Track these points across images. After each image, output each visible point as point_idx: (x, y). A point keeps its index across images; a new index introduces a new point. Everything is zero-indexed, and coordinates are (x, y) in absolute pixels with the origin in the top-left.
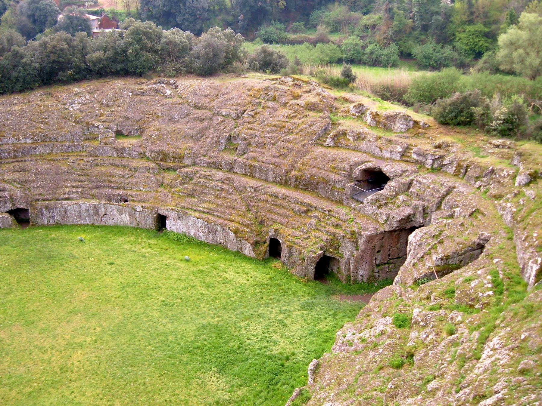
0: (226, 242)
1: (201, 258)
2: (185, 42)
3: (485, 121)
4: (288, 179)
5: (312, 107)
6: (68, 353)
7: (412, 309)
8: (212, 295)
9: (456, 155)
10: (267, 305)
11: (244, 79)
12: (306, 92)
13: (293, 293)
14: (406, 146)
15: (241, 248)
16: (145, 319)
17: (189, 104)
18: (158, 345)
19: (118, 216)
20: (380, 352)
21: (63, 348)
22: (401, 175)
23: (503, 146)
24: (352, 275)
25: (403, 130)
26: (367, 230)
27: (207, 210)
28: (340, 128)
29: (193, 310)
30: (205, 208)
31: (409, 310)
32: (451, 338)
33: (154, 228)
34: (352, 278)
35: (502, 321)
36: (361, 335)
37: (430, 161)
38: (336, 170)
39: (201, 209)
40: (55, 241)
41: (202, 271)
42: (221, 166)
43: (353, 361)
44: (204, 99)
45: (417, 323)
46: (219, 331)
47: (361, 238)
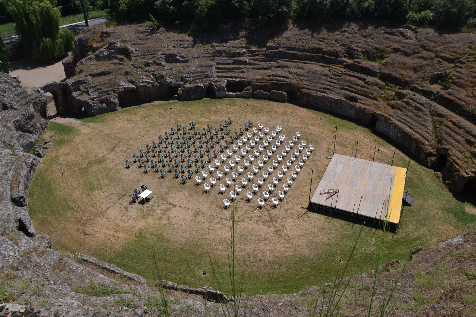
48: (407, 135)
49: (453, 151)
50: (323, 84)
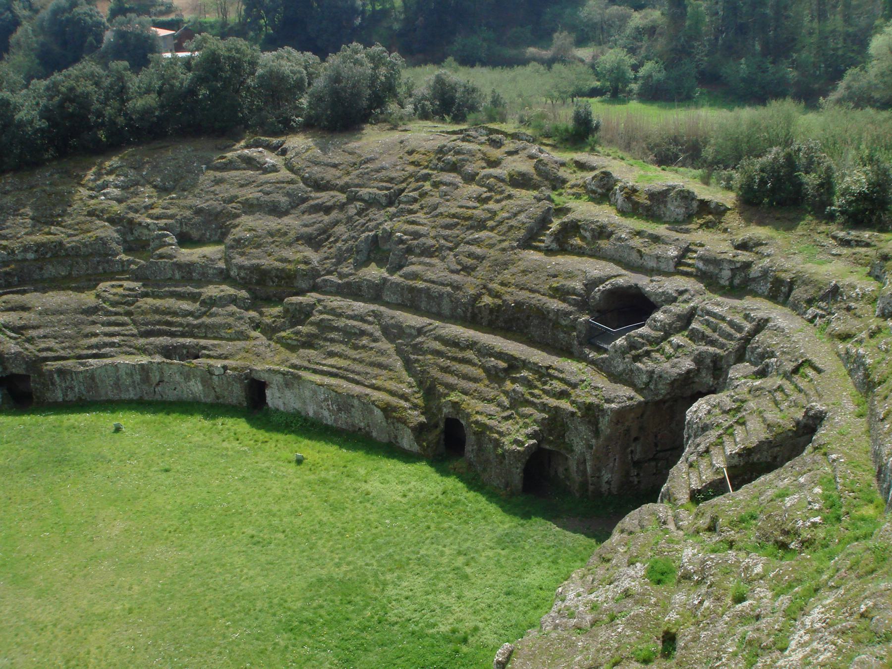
0: (368, 426)
1: (325, 456)
2: (300, 72)
3: (825, 198)
4: (476, 311)
5: (521, 181)
6: (82, 631)
7: (682, 550)
8: (339, 525)
9: (771, 261)
10: (435, 540)
11: (403, 133)
12: (510, 153)
13: (484, 518)
14: (685, 246)
15: (396, 437)
16: (218, 570)
17: (305, 181)
18: (237, 616)
19: (183, 385)
20: (619, 630)
21: (73, 624)
22: (675, 300)
23: (856, 241)
24: (590, 482)
25: (681, 218)
26: (613, 402)
27: (335, 370)
28: (570, 217)
29: (303, 551)
30: (332, 366)
31: (677, 551)
32: (739, 607)
33: (245, 404)
34: (591, 488)
35: (831, 577)
36: (592, 596)
37: (726, 273)
38: (560, 293)
39: (325, 368)
40: (73, 430)
41: (324, 482)
42: (360, 291)
43: (572, 645)
44: (333, 171)
45: (687, 577)
46: (346, 589)
47: (603, 416)
48: (344, 403)
49: (473, 405)
50: (96, 335)
